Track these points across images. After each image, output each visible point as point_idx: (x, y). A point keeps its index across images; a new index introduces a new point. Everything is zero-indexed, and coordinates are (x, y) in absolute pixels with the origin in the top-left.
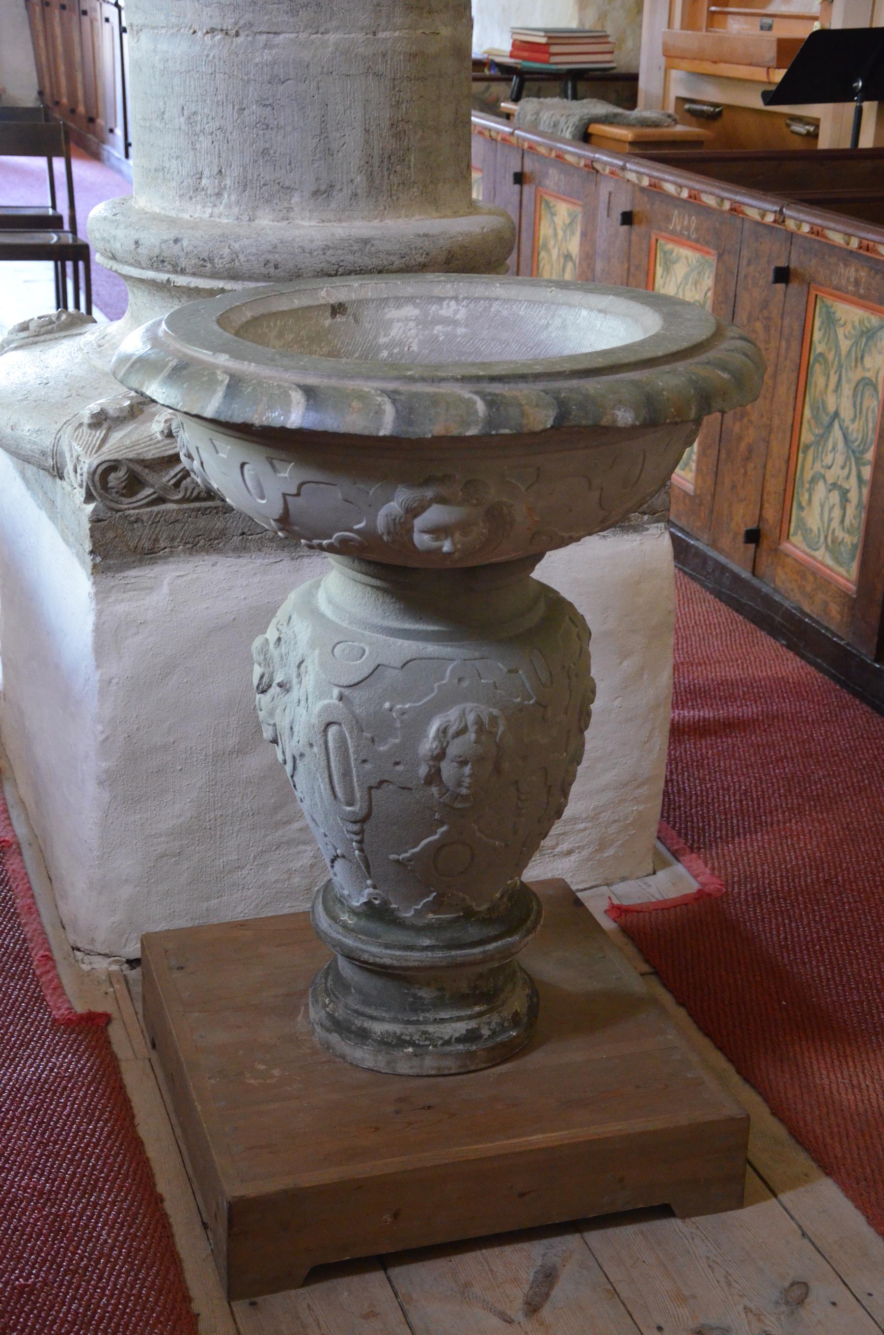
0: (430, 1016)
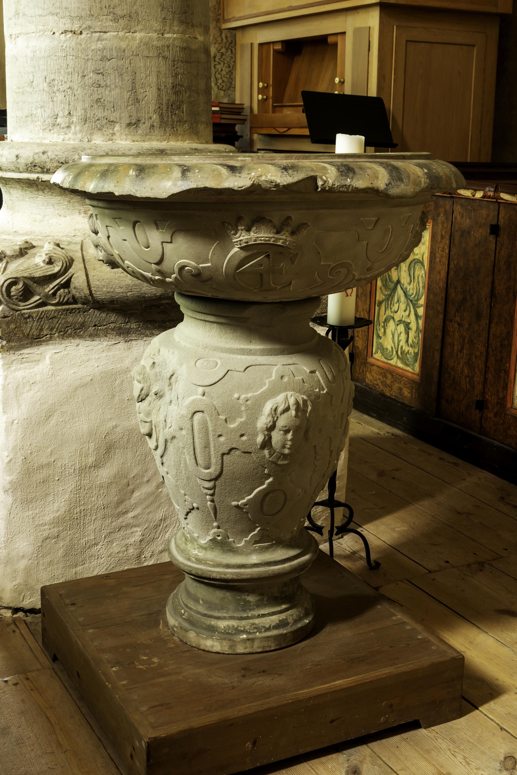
0: (256, 613)
